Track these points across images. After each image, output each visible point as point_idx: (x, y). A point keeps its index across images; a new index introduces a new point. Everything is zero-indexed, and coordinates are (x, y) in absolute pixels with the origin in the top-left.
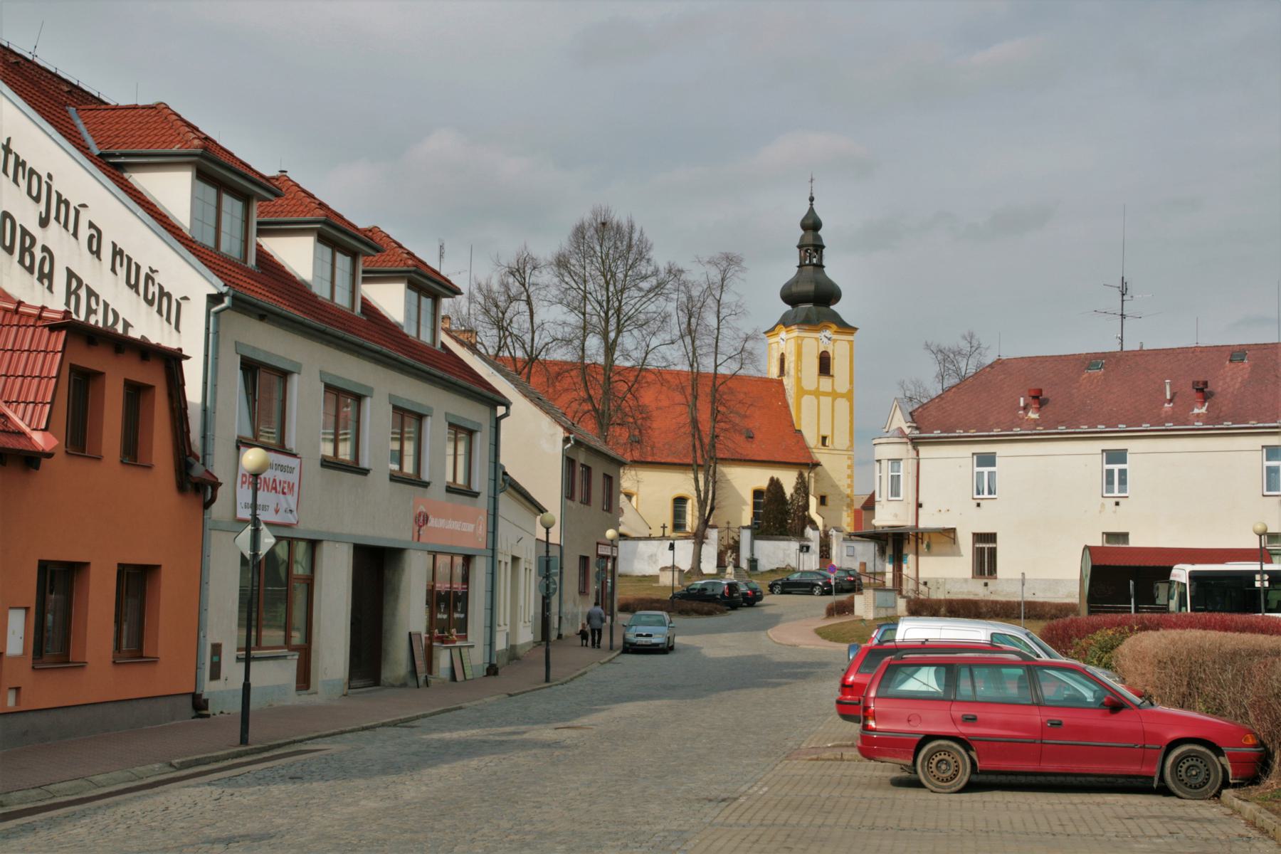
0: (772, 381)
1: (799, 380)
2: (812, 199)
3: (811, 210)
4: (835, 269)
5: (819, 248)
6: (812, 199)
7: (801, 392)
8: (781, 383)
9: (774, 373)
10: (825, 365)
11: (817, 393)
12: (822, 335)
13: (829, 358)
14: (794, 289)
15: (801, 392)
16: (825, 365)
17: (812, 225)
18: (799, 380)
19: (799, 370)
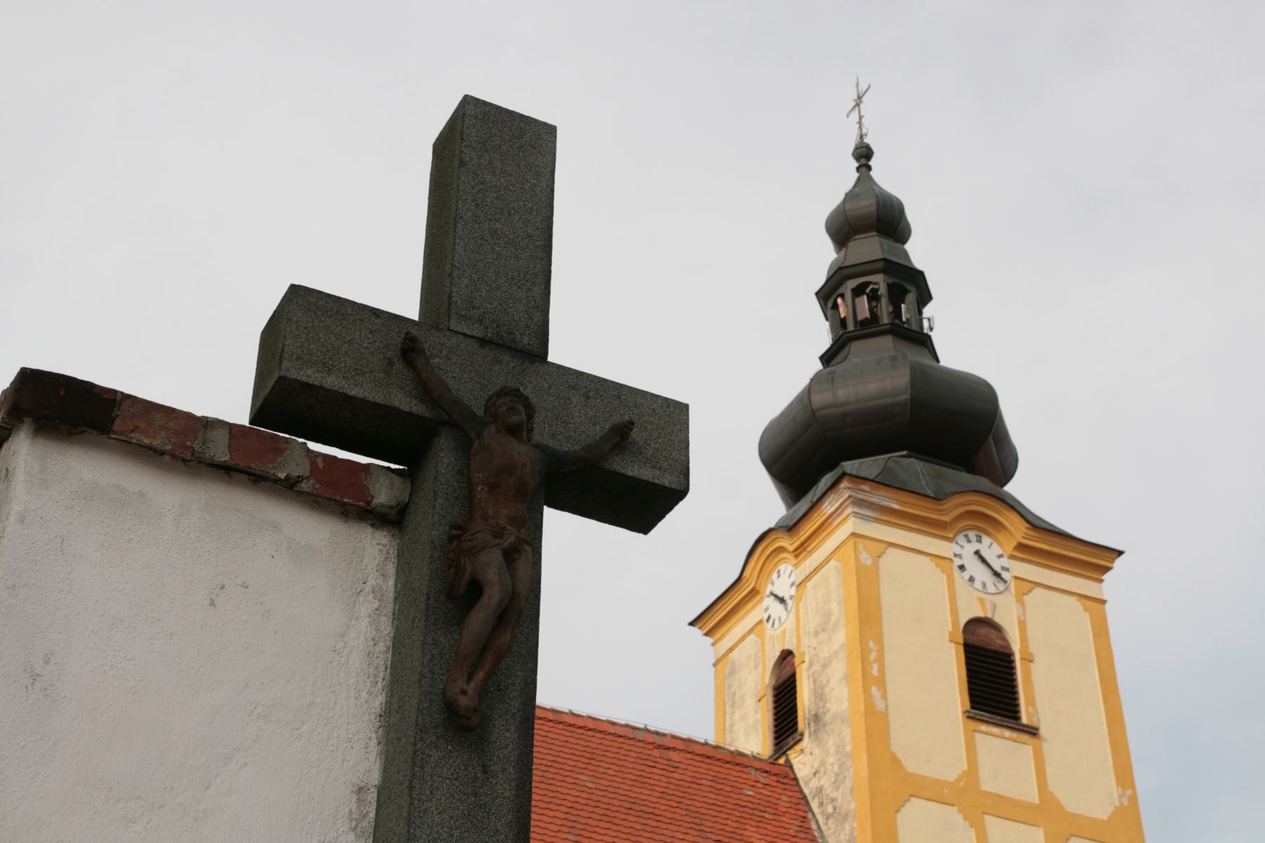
0: (738, 760)
1: (876, 725)
2: (864, 155)
3: (861, 137)
4: (960, 337)
5: (910, 285)
6: (864, 155)
7: (892, 785)
8: (789, 778)
9: (754, 739)
10: (991, 681)
11: (971, 799)
12: (964, 549)
13: (1006, 659)
14: (818, 400)
15: (892, 785)
16: (991, 681)
17: (871, 228)
18: (876, 725)
19: (870, 675)
